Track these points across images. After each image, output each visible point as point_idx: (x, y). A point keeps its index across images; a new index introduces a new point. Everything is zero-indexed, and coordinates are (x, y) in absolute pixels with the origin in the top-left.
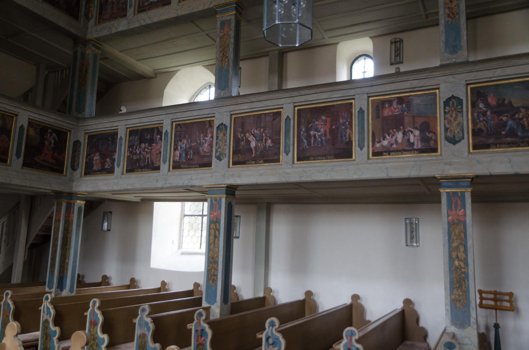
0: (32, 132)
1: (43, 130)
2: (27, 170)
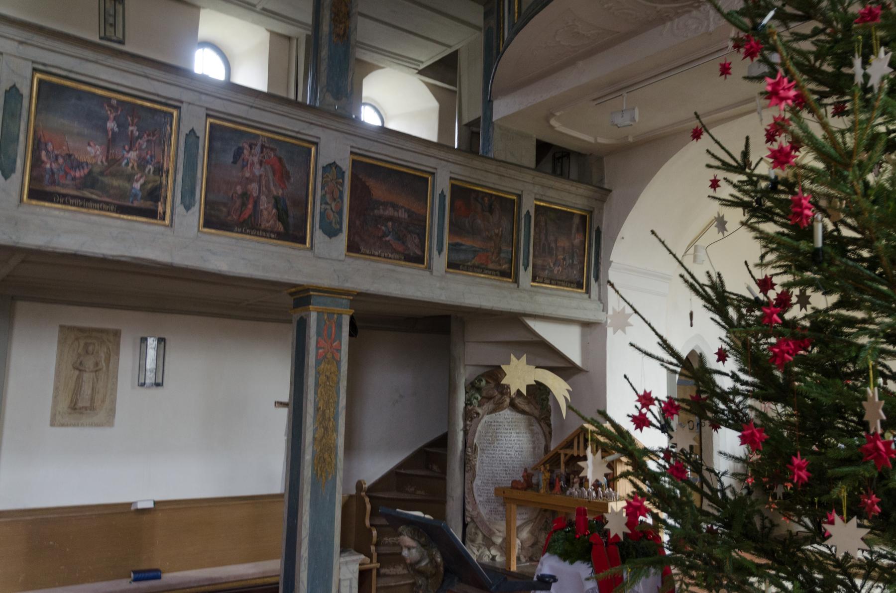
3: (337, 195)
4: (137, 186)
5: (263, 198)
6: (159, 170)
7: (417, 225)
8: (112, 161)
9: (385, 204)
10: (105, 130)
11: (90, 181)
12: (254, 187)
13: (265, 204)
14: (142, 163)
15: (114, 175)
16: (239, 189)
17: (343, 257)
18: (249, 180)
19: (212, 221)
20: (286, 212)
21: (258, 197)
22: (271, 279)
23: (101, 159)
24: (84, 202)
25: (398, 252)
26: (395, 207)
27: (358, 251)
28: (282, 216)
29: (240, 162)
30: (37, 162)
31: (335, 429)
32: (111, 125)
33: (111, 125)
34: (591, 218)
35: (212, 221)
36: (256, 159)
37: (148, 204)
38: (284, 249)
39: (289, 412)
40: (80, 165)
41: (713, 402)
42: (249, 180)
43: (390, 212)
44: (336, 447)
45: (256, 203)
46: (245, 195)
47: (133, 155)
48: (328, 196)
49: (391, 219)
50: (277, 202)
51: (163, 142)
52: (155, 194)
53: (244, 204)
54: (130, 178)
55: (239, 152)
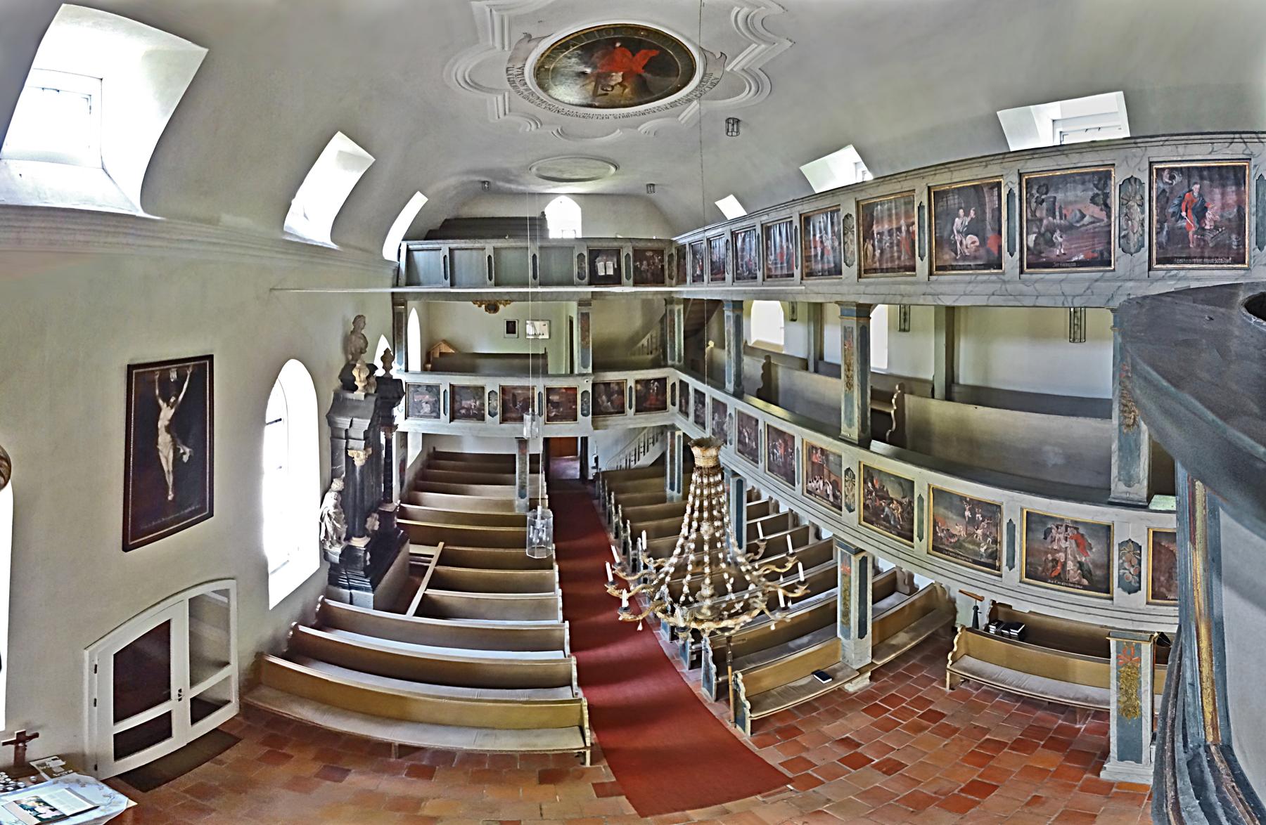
0: (639, 387)
1: (646, 383)
3: (1135, 562)
4: (982, 550)
6: (995, 542)
8: (970, 535)
10: (964, 517)
12: (1061, 556)
13: (1070, 565)
14: (985, 536)
16: (1050, 557)
18: (1058, 551)
20: (1090, 572)
21: (1065, 562)
23: (963, 533)
24: (957, 555)
29: (1049, 539)
30: (935, 532)
32: (967, 513)
33: (967, 513)
34: (1021, 266)
36: (1062, 536)
37: (990, 561)
38: (1094, 599)
39: (778, 346)
40: (954, 536)
41: (1211, 192)
42: (1058, 551)
45: (1064, 565)
46: (1055, 561)
47: (979, 532)
48: (1126, 565)
50: (1081, 565)
51: (997, 525)
52: (994, 555)
54: (979, 545)
55: (1047, 533)
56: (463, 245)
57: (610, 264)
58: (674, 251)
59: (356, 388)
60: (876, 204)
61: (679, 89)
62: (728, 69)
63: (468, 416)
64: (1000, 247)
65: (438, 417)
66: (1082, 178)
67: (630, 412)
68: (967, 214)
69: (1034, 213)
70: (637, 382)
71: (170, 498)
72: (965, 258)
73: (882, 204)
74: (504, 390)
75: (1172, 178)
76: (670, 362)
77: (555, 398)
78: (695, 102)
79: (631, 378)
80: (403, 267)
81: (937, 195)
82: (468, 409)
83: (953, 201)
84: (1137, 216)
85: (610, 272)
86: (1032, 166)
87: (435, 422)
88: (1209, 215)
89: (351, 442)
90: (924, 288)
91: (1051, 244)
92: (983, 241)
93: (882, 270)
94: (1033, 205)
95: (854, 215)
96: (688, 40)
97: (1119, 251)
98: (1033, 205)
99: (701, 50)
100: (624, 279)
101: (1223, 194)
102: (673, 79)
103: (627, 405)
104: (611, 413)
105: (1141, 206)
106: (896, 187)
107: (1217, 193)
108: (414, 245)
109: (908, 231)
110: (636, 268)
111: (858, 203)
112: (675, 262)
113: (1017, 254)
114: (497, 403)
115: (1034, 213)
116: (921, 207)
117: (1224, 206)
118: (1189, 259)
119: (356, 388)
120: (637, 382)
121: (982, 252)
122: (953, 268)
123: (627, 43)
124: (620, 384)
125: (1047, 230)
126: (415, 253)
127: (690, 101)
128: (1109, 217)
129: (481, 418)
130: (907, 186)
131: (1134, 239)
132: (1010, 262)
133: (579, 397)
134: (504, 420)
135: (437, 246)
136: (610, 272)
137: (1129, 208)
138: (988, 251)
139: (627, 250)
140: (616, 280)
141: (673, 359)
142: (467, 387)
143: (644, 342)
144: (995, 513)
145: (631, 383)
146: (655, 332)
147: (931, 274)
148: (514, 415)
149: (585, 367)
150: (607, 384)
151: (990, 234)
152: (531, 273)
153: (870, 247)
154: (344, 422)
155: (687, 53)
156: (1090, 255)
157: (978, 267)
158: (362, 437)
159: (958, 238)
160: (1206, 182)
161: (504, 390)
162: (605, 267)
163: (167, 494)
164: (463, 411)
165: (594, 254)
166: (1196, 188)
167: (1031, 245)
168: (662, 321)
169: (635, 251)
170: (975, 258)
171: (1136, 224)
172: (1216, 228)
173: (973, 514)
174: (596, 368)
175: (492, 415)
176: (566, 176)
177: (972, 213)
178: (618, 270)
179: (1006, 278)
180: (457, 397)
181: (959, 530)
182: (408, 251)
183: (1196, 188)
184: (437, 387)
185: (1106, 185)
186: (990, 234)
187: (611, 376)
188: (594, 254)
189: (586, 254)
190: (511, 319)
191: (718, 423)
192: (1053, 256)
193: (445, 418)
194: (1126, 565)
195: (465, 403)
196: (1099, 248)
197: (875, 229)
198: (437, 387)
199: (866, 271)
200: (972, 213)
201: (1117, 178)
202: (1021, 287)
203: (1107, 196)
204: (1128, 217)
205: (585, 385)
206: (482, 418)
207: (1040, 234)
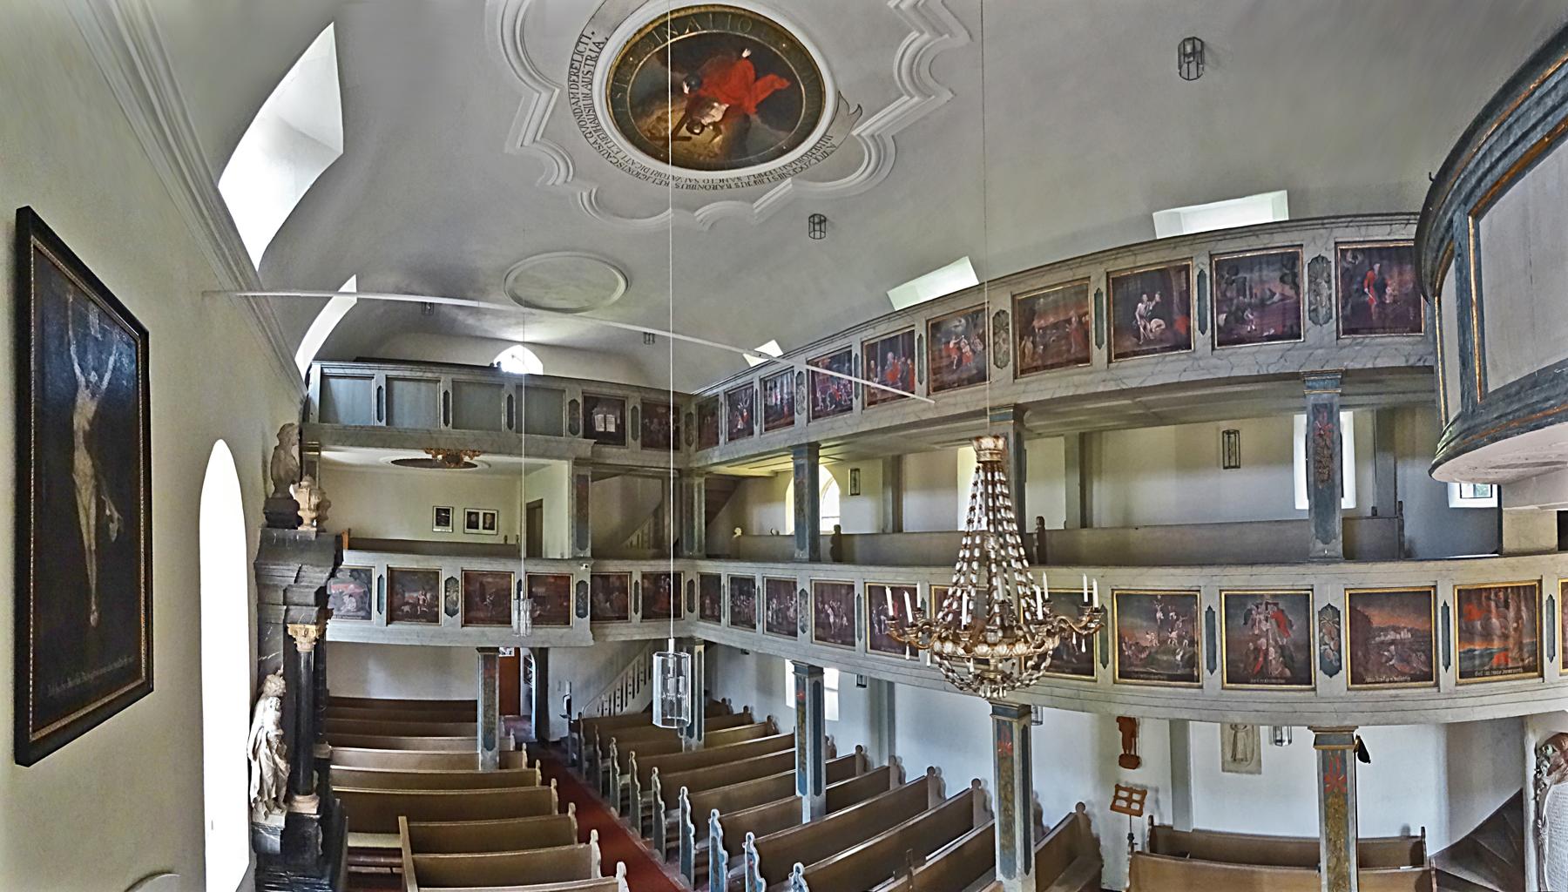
2: (647, 623)
5: (1271, 650)
7: (1424, 643)
8: (1163, 642)
9: (1385, 630)
11: (1151, 660)
15: (1164, 653)
17: (1344, 692)
18: (1258, 637)
19: (644, 446)
20: (1292, 658)
22: (401, 556)
23: (1155, 642)
24: (1148, 676)
25: (1403, 674)
26: (1397, 630)
27: (1363, 682)
28: (1288, 660)
31: (1347, 859)
32: (1159, 615)
33: (1159, 615)
35: (644, 446)
40: (1144, 648)
43: (1391, 636)
44: (1349, 875)
45: (1266, 653)
46: (1257, 649)
47: (1174, 634)
48: (1326, 639)
49: (1393, 642)
50: (1282, 649)
51: (1192, 620)
52: (1191, 662)
53: (1256, 659)
54: (1174, 653)
56: (408, 374)
57: (611, 418)
58: (693, 409)
59: (300, 521)
60: (1038, 297)
61: (782, 153)
62: (855, 133)
63: (413, 616)
64: (1189, 328)
65: (368, 617)
66: (1268, 260)
67: (636, 617)
68: (1151, 299)
69: (1224, 294)
70: (644, 576)
71: (93, 618)
72: (1148, 341)
73: (1045, 296)
74: (467, 576)
75: (1355, 257)
76: (686, 552)
77: (540, 590)
78: (789, 180)
79: (636, 570)
80: (316, 398)
81: (1115, 282)
82: (414, 605)
83: (1133, 287)
84: (1325, 293)
85: (612, 429)
86: (1222, 247)
87: (364, 624)
88: (1389, 290)
89: (294, 611)
90: (1104, 375)
91: (1244, 322)
92: (1170, 324)
93: (1045, 367)
94: (1224, 286)
95: (1009, 312)
96: (832, 75)
97: (1309, 323)
98: (1224, 286)
99: (839, 95)
100: (629, 439)
101: (1400, 274)
102: (782, 134)
103: (632, 606)
104: (610, 619)
105: (1329, 282)
106: (1066, 275)
107: (1395, 271)
108: (333, 369)
109: (1080, 321)
110: (644, 426)
111: (1013, 297)
112: (695, 424)
113: (1209, 332)
114: (459, 597)
115: (1224, 294)
116: (1098, 295)
117: (1401, 284)
118: (1371, 330)
119: (300, 521)
120: (644, 576)
121: (1169, 334)
122: (1136, 354)
123: (765, 63)
124: (623, 577)
125: (1238, 308)
126: (332, 380)
127: (783, 177)
128: (1298, 294)
129: (434, 619)
130: (1081, 273)
131: (1322, 312)
132: (1200, 340)
133: (573, 589)
134: (467, 622)
135: (368, 372)
136: (612, 429)
137: (1318, 285)
138: (1176, 334)
139: (634, 401)
140: (618, 439)
141: (692, 549)
142: (414, 572)
143: (634, 539)
144: (1191, 606)
145: (637, 577)
146: (647, 527)
147: (1110, 361)
148: (481, 615)
149: (582, 548)
150: (606, 577)
151: (1177, 317)
152: (504, 419)
153: (1029, 345)
154: (285, 572)
155: (821, 94)
156: (1280, 329)
157: (1164, 350)
158: (311, 599)
159: (1141, 323)
160: (1385, 262)
161: (467, 576)
162: (605, 422)
163: (88, 612)
164: (406, 608)
165: (592, 402)
166: (1377, 266)
167: (1222, 323)
168: (656, 511)
169: (643, 404)
170: (1161, 341)
171: (1324, 299)
172: (1395, 302)
173: (1166, 614)
174: (597, 555)
175: (450, 613)
176: (547, 301)
177: (1157, 297)
178: (621, 427)
179: (1197, 355)
180: (398, 587)
181: (1150, 639)
182: (323, 376)
183: (1377, 266)
184: (367, 572)
185: (1294, 265)
186: (1177, 317)
187: (613, 567)
188: (592, 402)
189: (580, 401)
190: (442, 505)
191: (777, 612)
192: (1243, 332)
193: (379, 617)
194: (1326, 639)
195: (411, 596)
196: (1288, 323)
197: (1036, 323)
198: (367, 572)
199: (1023, 372)
200: (1157, 297)
201: (1307, 257)
202: (1214, 361)
203: (1295, 275)
204: (1318, 294)
205: (582, 573)
206: (434, 619)
207: (1229, 314)
